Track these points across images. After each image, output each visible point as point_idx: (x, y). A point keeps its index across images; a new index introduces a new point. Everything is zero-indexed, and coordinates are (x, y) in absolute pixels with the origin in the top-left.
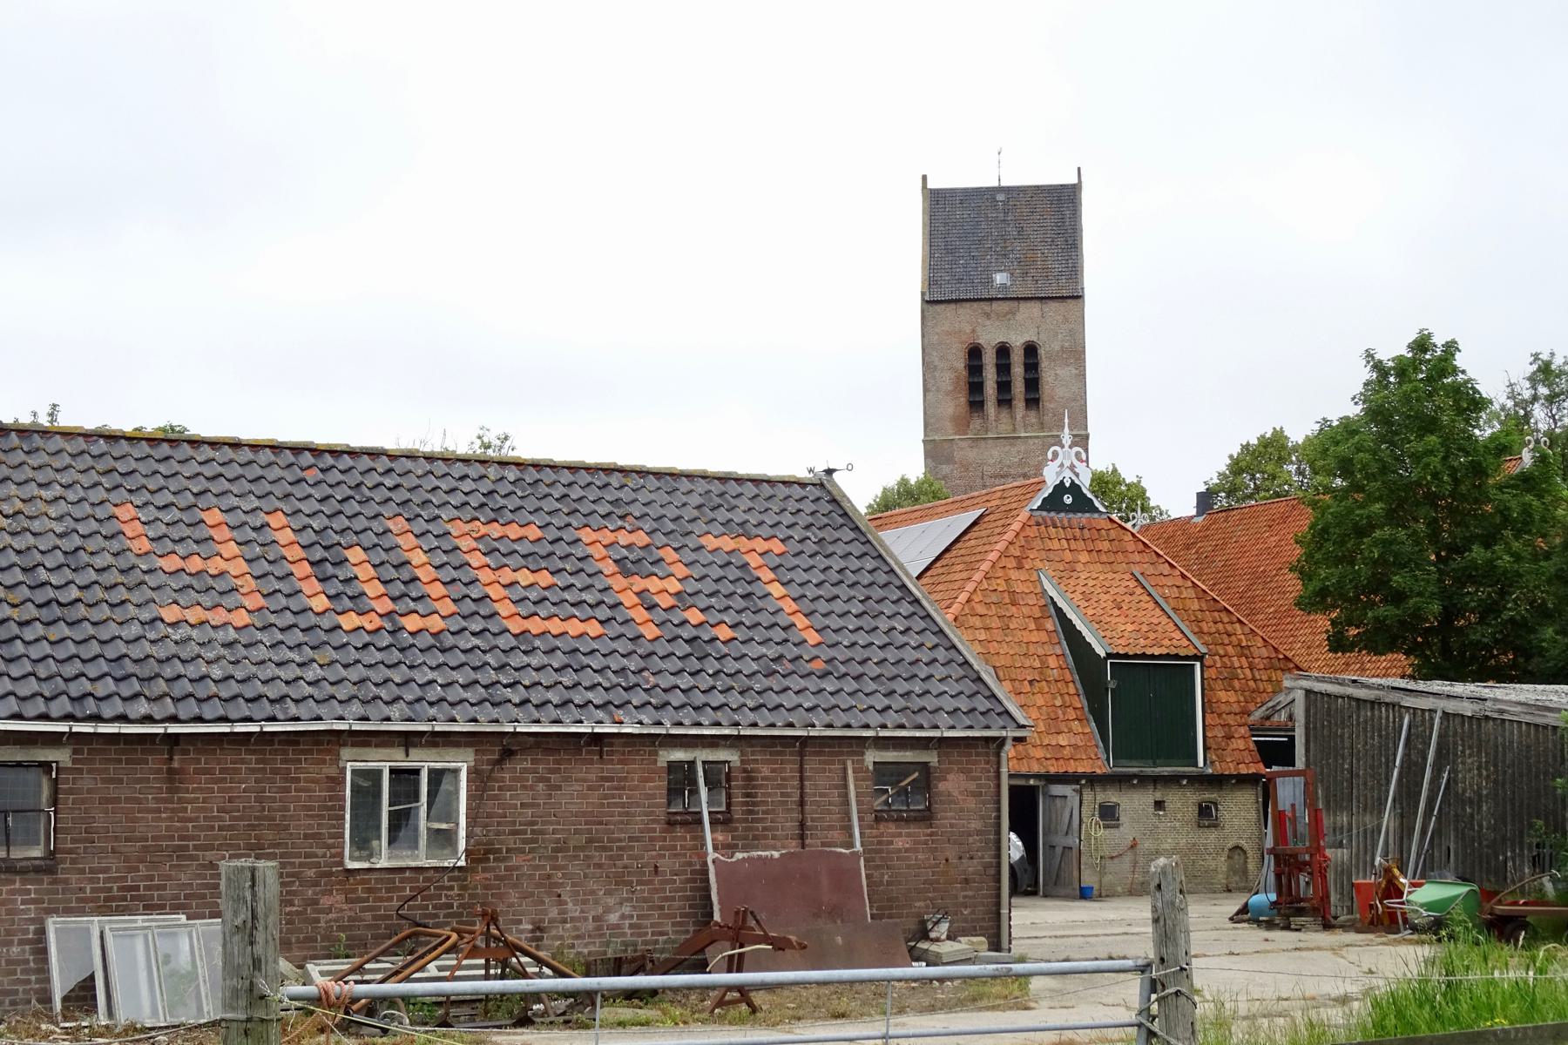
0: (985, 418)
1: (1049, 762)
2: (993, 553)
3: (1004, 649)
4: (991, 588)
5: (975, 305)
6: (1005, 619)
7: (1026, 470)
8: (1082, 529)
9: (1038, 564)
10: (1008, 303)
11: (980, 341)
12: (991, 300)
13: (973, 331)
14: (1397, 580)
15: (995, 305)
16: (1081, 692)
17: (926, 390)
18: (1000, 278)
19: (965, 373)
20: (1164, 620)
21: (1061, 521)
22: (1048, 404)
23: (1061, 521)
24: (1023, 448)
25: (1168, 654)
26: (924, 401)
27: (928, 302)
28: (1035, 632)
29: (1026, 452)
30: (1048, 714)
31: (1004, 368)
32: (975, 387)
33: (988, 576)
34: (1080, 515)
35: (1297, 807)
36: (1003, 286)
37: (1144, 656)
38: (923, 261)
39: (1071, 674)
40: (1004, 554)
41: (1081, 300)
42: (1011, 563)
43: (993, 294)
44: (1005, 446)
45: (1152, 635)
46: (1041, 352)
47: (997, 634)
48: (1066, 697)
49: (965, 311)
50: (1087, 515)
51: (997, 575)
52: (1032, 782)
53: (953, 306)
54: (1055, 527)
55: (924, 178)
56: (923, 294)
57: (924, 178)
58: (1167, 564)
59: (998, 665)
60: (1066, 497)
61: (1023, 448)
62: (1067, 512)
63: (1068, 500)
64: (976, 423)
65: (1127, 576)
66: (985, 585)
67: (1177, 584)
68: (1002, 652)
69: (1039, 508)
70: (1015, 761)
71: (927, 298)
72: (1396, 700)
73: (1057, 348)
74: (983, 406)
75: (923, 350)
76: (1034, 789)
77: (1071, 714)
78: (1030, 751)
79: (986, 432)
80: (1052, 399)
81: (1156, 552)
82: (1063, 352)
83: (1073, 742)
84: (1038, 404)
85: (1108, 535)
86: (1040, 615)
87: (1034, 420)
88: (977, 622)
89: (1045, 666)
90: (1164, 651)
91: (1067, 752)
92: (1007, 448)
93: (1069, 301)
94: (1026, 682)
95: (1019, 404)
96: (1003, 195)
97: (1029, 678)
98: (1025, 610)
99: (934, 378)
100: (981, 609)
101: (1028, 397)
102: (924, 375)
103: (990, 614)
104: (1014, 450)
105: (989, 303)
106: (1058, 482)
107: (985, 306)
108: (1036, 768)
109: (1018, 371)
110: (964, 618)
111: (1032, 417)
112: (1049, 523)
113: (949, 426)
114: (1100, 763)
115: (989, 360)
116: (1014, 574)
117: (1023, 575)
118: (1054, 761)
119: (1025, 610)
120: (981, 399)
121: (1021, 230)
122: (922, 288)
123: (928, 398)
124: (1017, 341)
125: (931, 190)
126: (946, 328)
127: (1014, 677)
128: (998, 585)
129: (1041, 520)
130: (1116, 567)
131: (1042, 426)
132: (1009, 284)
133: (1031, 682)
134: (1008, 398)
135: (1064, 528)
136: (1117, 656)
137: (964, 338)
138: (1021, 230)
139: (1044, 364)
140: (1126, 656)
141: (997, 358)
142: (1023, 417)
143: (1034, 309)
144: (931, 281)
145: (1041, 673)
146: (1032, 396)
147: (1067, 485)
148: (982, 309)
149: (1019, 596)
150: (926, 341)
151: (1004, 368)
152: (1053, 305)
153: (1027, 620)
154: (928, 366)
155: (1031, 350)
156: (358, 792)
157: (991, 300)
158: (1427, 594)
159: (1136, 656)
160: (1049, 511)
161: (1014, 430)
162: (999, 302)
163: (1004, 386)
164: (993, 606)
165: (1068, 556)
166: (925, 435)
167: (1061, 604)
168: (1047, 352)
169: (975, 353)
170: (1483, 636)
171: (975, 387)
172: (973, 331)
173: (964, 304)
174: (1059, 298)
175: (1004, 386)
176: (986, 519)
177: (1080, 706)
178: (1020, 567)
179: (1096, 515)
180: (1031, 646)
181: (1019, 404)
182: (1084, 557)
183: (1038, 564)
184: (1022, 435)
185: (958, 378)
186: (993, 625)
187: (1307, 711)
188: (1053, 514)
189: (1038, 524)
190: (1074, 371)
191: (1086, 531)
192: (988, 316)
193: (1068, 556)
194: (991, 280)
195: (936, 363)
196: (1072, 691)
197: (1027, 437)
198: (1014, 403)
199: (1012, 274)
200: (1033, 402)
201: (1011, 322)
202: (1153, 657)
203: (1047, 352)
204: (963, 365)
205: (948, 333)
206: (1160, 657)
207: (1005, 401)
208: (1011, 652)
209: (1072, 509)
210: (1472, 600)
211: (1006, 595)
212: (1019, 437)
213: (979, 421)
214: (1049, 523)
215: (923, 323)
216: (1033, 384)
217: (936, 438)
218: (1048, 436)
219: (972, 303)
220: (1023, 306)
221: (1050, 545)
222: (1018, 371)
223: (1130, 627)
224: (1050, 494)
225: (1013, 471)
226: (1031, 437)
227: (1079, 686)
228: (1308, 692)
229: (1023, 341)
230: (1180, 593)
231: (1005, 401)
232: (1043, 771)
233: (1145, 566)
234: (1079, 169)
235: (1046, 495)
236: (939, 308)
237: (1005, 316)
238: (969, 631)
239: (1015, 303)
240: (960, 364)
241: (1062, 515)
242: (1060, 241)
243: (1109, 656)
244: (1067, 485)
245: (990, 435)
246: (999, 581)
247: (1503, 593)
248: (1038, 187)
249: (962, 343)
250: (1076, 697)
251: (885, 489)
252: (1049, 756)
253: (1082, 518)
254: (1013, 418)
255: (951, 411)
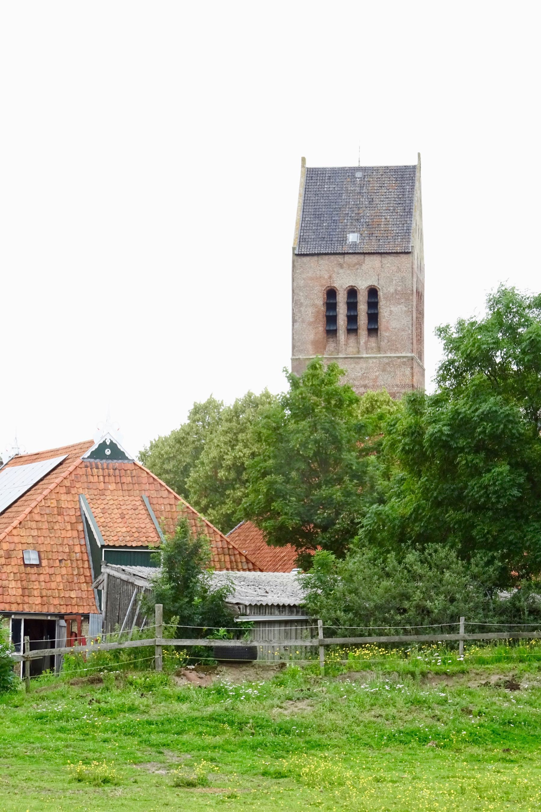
0: (337, 342)
1: (62, 607)
2: (53, 485)
3: (48, 541)
4: (47, 505)
5: (332, 257)
6: (52, 523)
7: (367, 382)
8: (115, 469)
9: (81, 491)
10: (357, 256)
11: (335, 285)
12: (344, 254)
13: (330, 277)
14: (275, 505)
15: (347, 257)
16: (92, 567)
17: (294, 321)
18: (352, 238)
19: (323, 309)
20: (149, 525)
21: (102, 465)
22: (384, 333)
23: (102, 465)
24: (364, 365)
25: (142, 546)
26: (293, 329)
27: (296, 255)
28: (70, 532)
29: (367, 368)
30: (67, 579)
31: (352, 305)
32: (331, 320)
33: (46, 498)
34: (115, 461)
35: (294, 637)
36: (355, 244)
37: (126, 547)
38: (297, 223)
39: (88, 557)
40: (59, 485)
41: (410, 255)
42: (63, 490)
43: (346, 249)
44: (351, 364)
45: (136, 535)
46: (380, 294)
47: (46, 533)
48: (82, 570)
49: (324, 261)
50: (120, 461)
51: (52, 498)
52: (49, 618)
53: (315, 258)
54: (97, 468)
55: (303, 160)
56: (294, 249)
57: (303, 160)
58: (166, 491)
59: (42, 550)
60: (106, 450)
61: (364, 365)
62: (107, 459)
63: (108, 452)
64: (331, 346)
65: (138, 498)
66: (43, 503)
67: (171, 503)
68: (46, 543)
69: (88, 457)
70: (40, 606)
71: (296, 252)
72: (133, 581)
73: (392, 290)
74: (336, 334)
75: (293, 291)
76: (54, 622)
77: (82, 579)
78: (51, 600)
79: (338, 353)
80: (387, 329)
81: (160, 484)
82: (397, 294)
83: (80, 595)
84: (377, 333)
85: (131, 473)
86: (75, 521)
87: (374, 345)
88: (34, 525)
89: (71, 551)
90: (139, 544)
91: (74, 602)
92: (353, 366)
93: (402, 255)
94: (57, 561)
95: (363, 332)
96: (361, 173)
97: (60, 558)
98: (67, 518)
99: (300, 312)
100: (37, 518)
101: (370, 327)
102: (293, 310)
103: (43, 520)
104: (358, 367)
105: (342, 256)
106: (102, 442)
107: (340, 259)
108: (52, 610)
109: (363, 308)
110: (26, 522)
111: (373, 343)
112: (94, 466)
113: (310, 347)
114: (94, 607)
115: (342, 299)
116: (64, 497)
117: (69, 497)
118: (65, 606)
119: (67, 518)
120: (335, 328)
121: (371, 201)
122: (294, 244)
123: (295, 327)
124: (362, 286)
125: (308, 168)
126: (310, 275)
127: (50, 557)
128: (51, 503)
129: (88, 464)
130: (132, 493)
131: (379, 349)
132: (358, 242)
133: (60, 561)
134: (355, 327)
135: (103, 469)
136: (108, 546)
137: (323, 282)
138: (371, 201)
139: (382, 303)
140: (114, 547)
141: (348, 299)
142: (366, 343)
143: (375, 261)
144: (302, 239)
145: (69, 555)
146: (373, 327)
147: (108, 443)
148: (338, 261)
149: (64, 510)
150: (295, 284)
151: (352, 305)
152: (390, 258)
153: (66, 524)
154: (296, 303)
155: (373, 292)
156: (183, 621)
157: (344, 254)
158: (290, 514)
159: (120, 547)
160: (95, 459)
161: (358, 352)
162: (350, 256)
163: (352, 319)
164: (45, 516)
165: (102, 486)
166: (293, 355)
167: (87, 515)
168: (384, 294)
169: (331, 293)
170: (324, 539)
171: (331, 320)
172: (330, 277)
173: (324, 257)
174: (394, 253)
175: (352, 319)
176: (67, 462)
177: (89, 575)
178: (68, 493)
179: (126, 461)
180: (65, 539)
181: (363, 332)
182: (112, 487)
183: (81, 491)
184: (364, 356)
185: (318, 312)
186: (44, 527)
187: (108, 584)
188: (98, 460)
189: (86, 467)
190: (404, 309)
191: (117, 471)
192: (341, 266)
193: (102, 486)
194: (345, 239)
195: (302, 301)
196: (86, 565)
197: (367, 358)
198: (359, 331)
199: (361, 234)
200: (373, 331)
201: (359, 271)
202: (132, 547)
203: (384, 294)
204: (322, 303)
205: (312, 279)
206: (136, 547)
207: (352, 330)
208: (52, 543)
209: (110, 457)
210: (318, 518)
211: (56, 509)
212: (362, 358)
213: (333, 345)
214: (94, 466)
215: (293, 271)
216: (373, 318)
217: (301, 357)
218: (384, 357)
219: (330, 256)
220: (368, 258)
221: (91, 479)
222: (363, 308)
223: (124, 530)
224: (96, 450)
225: (356, 383)
226: (370, 358)
227: (91, 563)
228: (109, 575)
229: (366, 285)
230: (171, 508)
231: (352, 330)
232: (57, 612)
233: (152, 492)
234: (419, 155)
235: (94, 449)
236: (306, 259)
237: (354, 266)
238: (28, 530)
239: (362, 257)
240: (320, 301)
241: (104, 461)
242: (399, 210)
243: (103, 546)
244: (108, 443)
245: (341, 356)
246: (52, 501)
247: (338, 514)
248: (387, 168)
249: (322, 286)
250: (88, 570)
251: (237, 399)
252: (62, 603)
253: (116, 463)
254: (358, 343)
255: (312, 337)
